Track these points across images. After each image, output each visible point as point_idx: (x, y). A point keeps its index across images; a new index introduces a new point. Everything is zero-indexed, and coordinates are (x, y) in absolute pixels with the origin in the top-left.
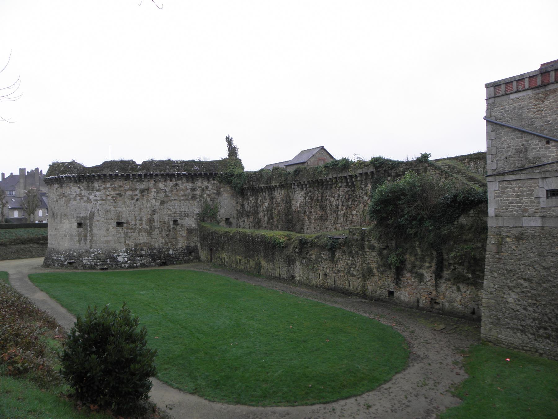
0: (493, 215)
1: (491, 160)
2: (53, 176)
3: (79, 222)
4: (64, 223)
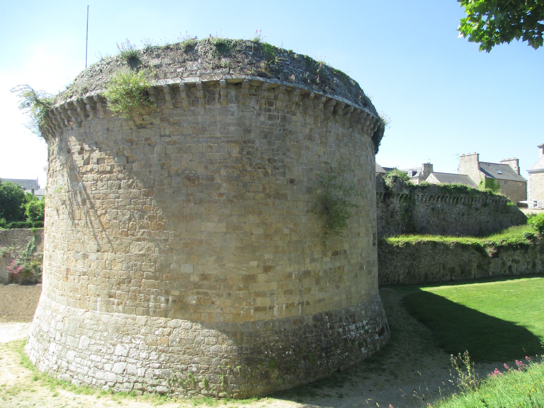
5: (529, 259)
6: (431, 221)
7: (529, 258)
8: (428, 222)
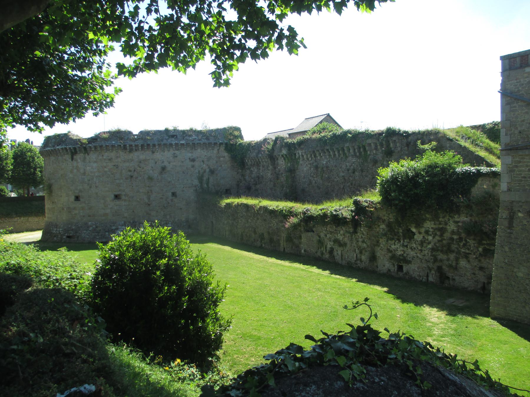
0: (505, 189)
1: (504, 134)
2: (49, 149)
3: (77, 195)
4: (61, 196)
5: (365, 245)
6: (314, 182)
7: (363, 242)
8: (310, 182)
